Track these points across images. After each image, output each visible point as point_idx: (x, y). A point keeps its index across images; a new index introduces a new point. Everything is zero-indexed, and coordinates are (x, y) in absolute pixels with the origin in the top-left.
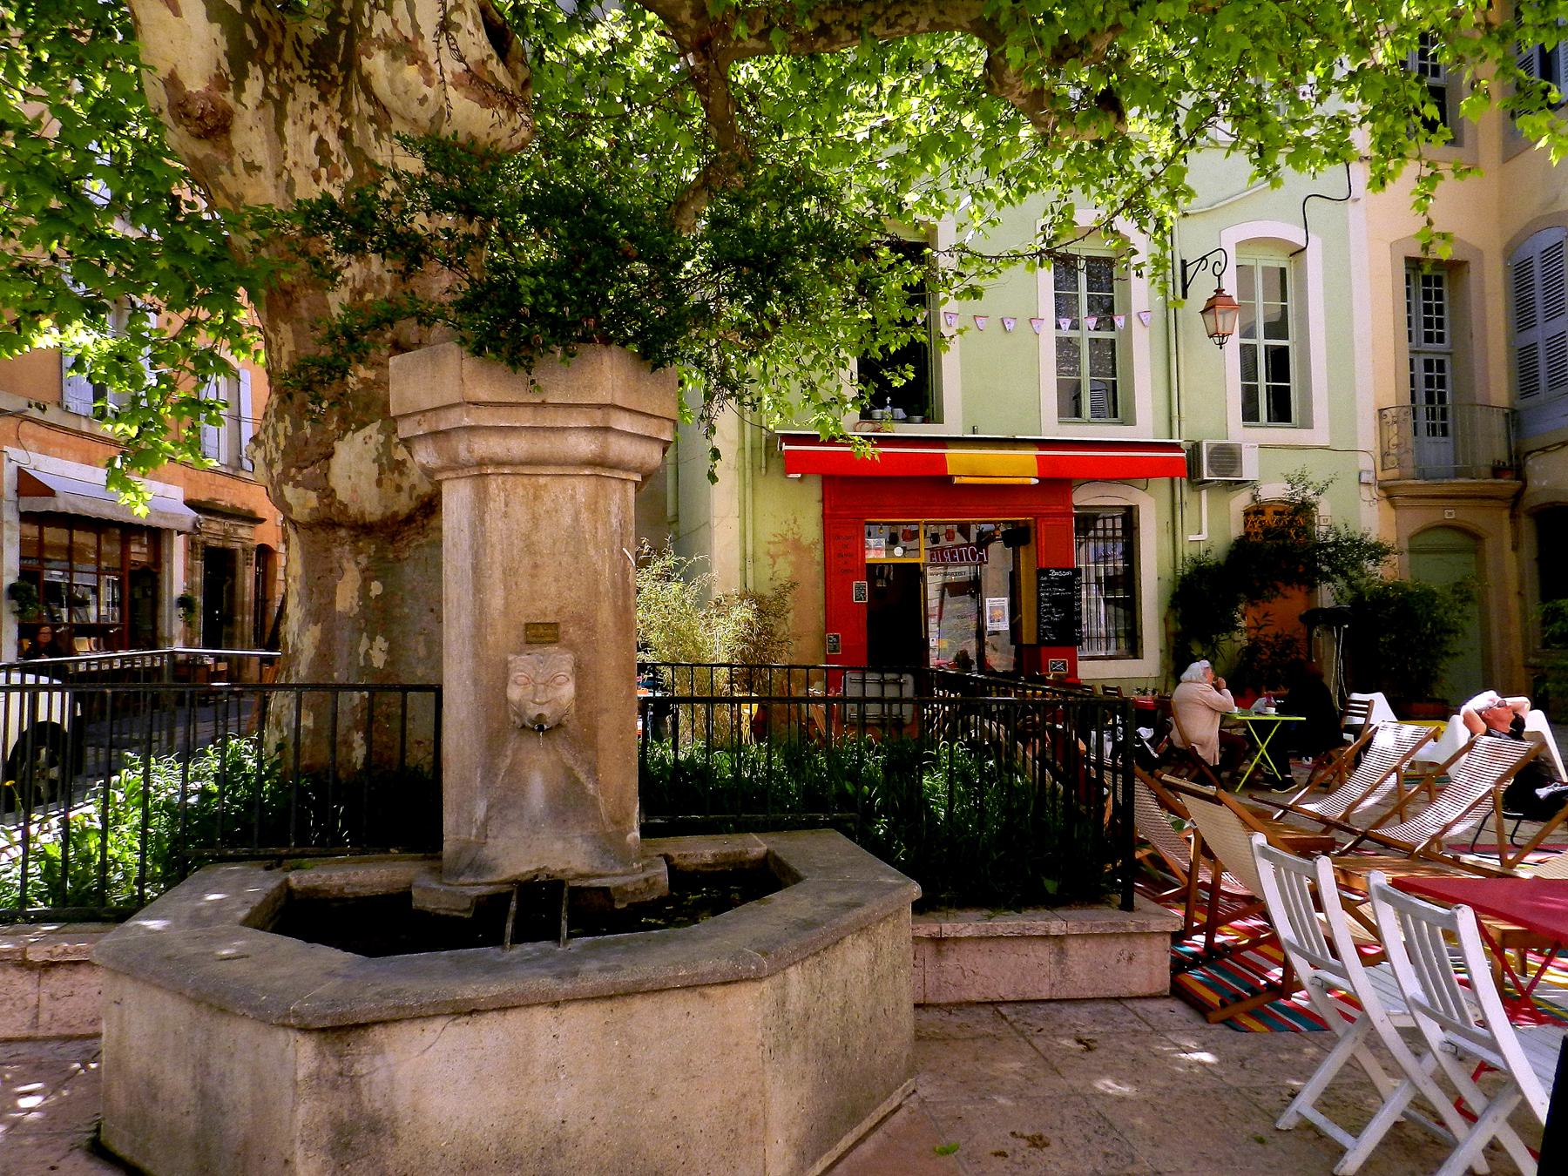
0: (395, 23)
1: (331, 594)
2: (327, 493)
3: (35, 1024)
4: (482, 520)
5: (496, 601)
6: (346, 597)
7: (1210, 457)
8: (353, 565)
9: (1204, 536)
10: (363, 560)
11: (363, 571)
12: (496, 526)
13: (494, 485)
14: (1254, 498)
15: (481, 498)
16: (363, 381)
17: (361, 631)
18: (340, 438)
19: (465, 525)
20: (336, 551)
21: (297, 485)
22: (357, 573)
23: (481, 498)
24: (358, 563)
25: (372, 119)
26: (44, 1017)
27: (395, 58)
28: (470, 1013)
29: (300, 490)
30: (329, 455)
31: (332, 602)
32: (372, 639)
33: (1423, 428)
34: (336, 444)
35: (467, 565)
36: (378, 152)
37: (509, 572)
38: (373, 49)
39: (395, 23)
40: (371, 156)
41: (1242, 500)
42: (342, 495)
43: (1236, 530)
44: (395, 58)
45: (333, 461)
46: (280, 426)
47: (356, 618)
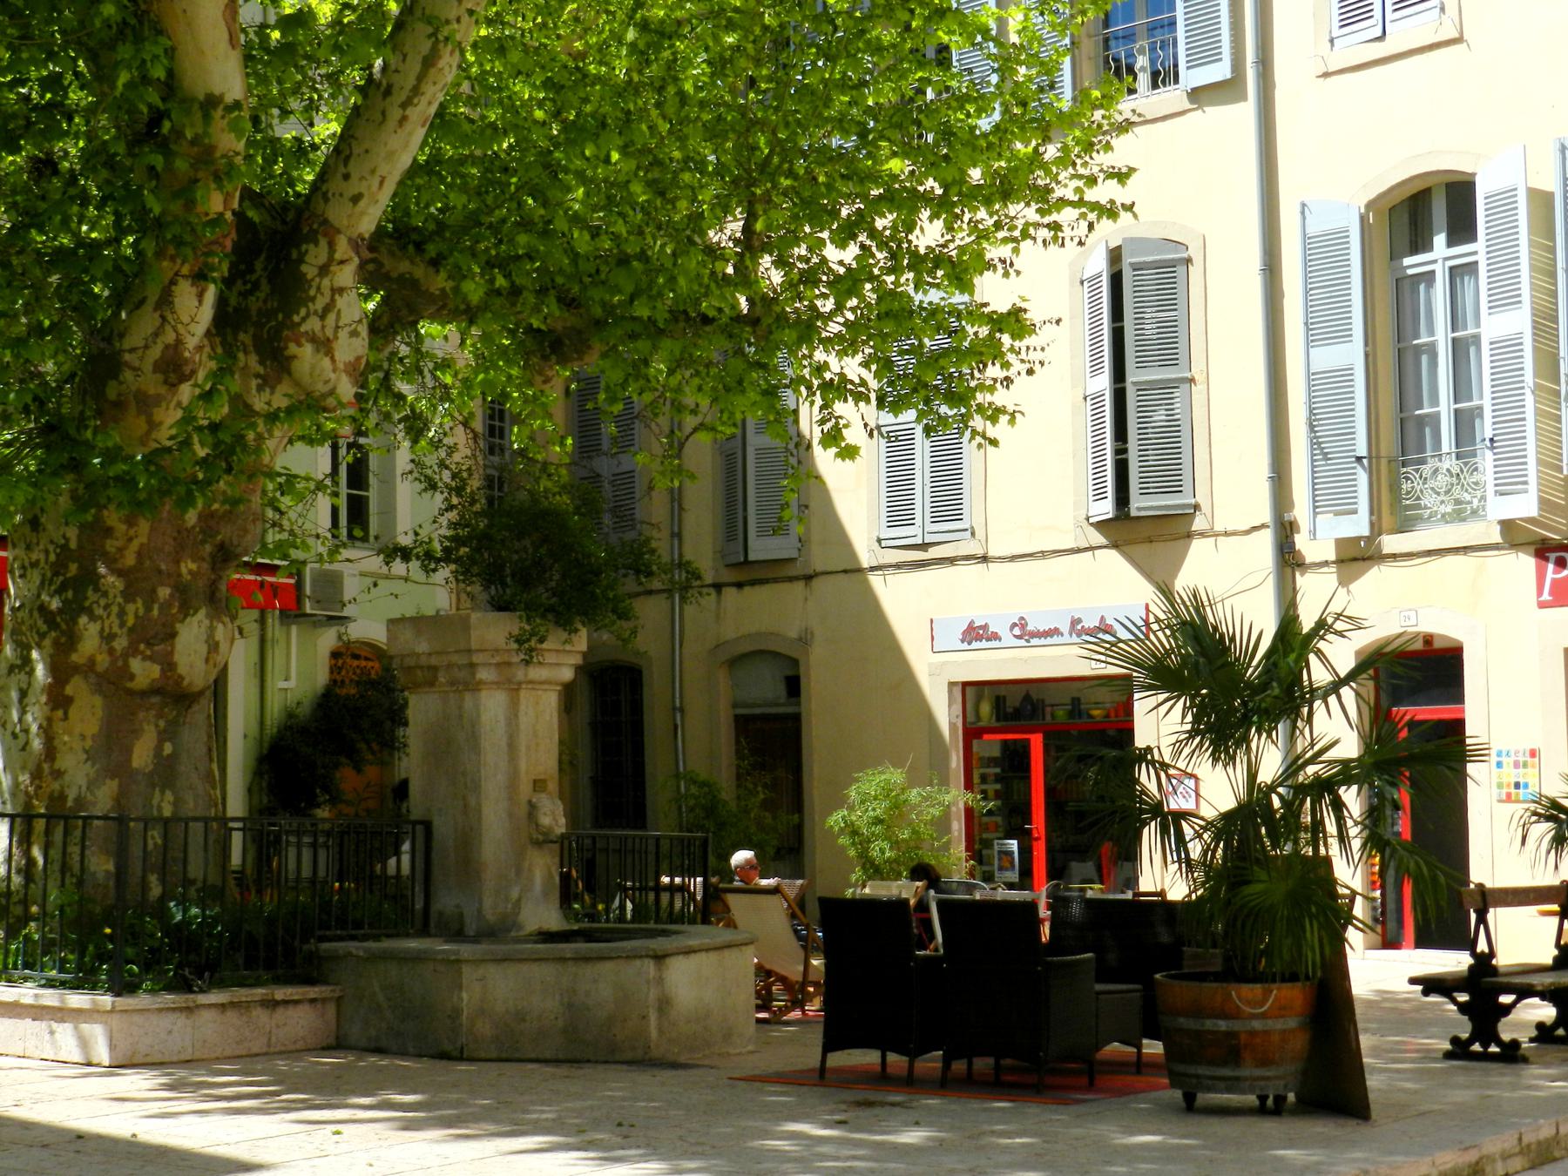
0: (323, 327)
1: (128, 752)
2: (169, 665)
3: (269, 1046)
4: (516, 716)
5: (523, 766)
6: (142, 756)
7: (313, 581)
8: (152, 728)
9: (292, 684)
10: (162, 723)
11: (159, 733)
12: (525, 720)
13: (523, 693)
14: (340, 637)
15: (514, 705)
16: (190, 572)
17: (153, 786)
18: (182, 621)
19: (502, 718)
20: (141, 715)
21: (145, 658)
22: (155, 735)
23: (514, 705)
24: (157, 726)
25: (257, 376)
26: (274, 1039)
27: (318, 351)
28: (444, 1056)
29: (148, 663)
30: (173, 635)
31: (129, 760)
32: (163, 793)
33: (1156, 751)
34: (178, 625)
35: (504, 743)
36: (256, 400)
37: (528, 748)
38: (303, 340)
39: (323, 327)
40: (249, 402)
41: (327, 639)
42: (182, 669)
43: (322, 677)
44: (318, 351)
45: (177, 640)
46: (131, 608)
47: (151, 774)
